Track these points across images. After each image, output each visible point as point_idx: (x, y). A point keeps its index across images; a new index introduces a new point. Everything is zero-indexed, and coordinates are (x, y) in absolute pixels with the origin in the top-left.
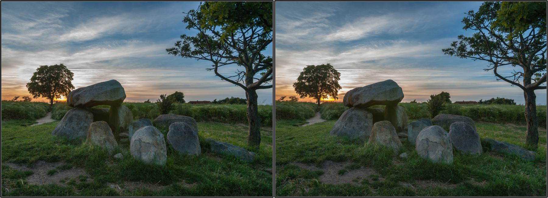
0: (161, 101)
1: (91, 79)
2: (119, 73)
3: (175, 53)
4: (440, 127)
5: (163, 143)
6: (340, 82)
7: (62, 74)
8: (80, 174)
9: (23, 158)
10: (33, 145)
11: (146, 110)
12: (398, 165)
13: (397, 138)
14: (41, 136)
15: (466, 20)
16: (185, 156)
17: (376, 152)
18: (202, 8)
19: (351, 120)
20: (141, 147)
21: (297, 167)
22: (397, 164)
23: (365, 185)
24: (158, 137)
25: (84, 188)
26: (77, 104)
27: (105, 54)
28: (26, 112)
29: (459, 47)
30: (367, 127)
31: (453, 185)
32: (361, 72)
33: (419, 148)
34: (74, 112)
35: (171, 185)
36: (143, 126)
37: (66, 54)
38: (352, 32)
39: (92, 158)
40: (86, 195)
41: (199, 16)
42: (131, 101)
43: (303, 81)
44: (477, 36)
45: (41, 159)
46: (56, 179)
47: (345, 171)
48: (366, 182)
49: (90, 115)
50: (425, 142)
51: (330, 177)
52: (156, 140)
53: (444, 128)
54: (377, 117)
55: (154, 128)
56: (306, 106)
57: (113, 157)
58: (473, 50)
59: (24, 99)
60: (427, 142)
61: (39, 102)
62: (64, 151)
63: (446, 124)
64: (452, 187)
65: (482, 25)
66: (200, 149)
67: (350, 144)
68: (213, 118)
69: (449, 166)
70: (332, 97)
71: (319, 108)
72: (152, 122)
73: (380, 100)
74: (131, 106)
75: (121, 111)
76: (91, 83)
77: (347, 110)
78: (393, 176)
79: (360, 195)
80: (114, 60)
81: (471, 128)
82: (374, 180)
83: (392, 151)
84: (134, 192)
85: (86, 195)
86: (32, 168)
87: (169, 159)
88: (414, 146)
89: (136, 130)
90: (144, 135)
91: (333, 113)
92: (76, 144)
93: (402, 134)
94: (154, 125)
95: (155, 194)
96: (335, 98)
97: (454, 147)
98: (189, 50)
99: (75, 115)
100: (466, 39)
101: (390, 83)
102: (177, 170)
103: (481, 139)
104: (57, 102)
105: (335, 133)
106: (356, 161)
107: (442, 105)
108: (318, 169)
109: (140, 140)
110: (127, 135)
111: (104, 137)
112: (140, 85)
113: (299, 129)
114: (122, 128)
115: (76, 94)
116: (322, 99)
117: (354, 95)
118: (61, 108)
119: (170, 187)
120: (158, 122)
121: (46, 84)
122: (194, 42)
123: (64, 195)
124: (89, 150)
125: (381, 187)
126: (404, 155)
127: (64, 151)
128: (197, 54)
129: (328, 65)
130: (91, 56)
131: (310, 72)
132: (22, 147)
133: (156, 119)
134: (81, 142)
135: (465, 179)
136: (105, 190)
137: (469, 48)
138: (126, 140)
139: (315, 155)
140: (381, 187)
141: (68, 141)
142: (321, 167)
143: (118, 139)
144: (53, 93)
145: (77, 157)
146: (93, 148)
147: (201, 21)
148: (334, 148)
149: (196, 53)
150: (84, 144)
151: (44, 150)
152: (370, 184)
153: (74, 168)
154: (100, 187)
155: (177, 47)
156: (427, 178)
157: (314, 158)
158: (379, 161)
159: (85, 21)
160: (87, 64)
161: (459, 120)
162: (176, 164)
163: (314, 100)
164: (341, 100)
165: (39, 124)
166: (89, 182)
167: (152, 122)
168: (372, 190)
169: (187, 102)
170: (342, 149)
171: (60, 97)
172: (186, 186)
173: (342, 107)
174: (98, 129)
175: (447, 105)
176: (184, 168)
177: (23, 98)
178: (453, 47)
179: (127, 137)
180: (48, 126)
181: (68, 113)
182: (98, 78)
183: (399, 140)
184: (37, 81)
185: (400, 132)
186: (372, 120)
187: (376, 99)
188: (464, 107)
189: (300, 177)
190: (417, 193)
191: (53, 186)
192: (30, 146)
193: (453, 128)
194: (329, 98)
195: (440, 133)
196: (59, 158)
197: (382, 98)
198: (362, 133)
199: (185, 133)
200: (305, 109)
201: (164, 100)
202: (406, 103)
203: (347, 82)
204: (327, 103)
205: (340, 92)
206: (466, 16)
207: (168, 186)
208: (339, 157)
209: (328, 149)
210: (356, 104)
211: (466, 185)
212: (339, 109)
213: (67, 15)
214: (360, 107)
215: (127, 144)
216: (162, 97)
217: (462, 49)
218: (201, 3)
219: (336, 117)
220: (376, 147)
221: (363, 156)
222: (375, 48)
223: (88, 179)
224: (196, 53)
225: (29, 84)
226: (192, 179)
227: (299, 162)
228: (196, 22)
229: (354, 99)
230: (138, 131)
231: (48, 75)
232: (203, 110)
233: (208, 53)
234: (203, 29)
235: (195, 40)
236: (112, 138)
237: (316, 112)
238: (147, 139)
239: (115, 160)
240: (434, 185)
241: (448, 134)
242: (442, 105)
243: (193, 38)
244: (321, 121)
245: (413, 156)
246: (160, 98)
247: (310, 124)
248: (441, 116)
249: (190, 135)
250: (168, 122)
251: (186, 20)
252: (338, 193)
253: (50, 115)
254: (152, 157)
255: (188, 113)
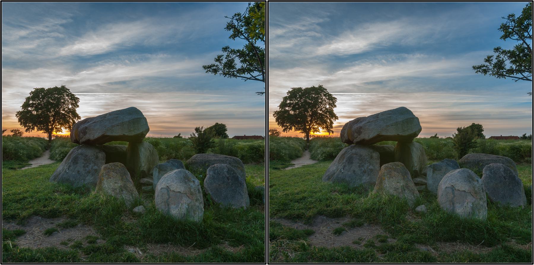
0: (197, 135)
1: (102, 106)
2: (140, 98)
3: (485, 72)
4: (470, 171)
5: (199, 192)
6: (336, 110)
7: (64, 99)
8: (88, 233)
9: (12, 213)
10: (25, 195)
11: (177, 149)
12: (413, 222)
13: (412, 185)
14: (36, 183)
15: (504, 27)
16: (228, 210)
17: (384, 204)
18: (251, 10)
19: (350, 161)
20: (454, 196)
21: (279, 225)
22: (412, 220)
23: (369, 249)
24: (192, 184)
25: (93, 252)
26: (84, 140)
27: (121, 72)
28: (277, 150)
29: (496, 64)
30: (372, 170)
31: (486, 249)
32: (364, 97)
33: (442, 199)
34: (80, 151)
35: (210, 249)
36: (172, 170)
37: (69, 72)
38: (95, 44)
39: (104, 213)
40: (96, 262)
41: (248, 22)
42: (156, 136)
43: (287, 108)
44: (520, 49)
45: (36, 213)
46: (55, 241)
47: (343, 230)
48: (371, 245)
49: (101, 155)
50: (450, 191)
51: (323, 237)
52: (190, 188)
53: (476, 173)
54: (386, 157)
55: (187, 171)
56: (291, 142)
57: (132, 211)
58: (514, 67)
59: (12, 133)
60: (453, 190)
61: (33, 137)
62: (66, 203)
63: (477, 167)
64: (485, 251)
65: (526, 34)
66: (248, 200)
67: (350, 194)
68: (526, 159)
69: (482, 223)
70: (325, 130)
71: (308, 145)
72: (184, 164)
73: (389, 134)
74: (155, 143)
75: (143, 150)
76: (102, 111)
77: (345, 148)
78: (407, 236)
79: (363, 261)
80: (390, 81)
81: (511, 172)
82: (382, 241)
83: (406, 203)
84: (160, 258)
85: (506, 261)
86: (23, 225)
87: (207, 213)
88: (436, 196)
89: (162, 175)
90: (173, 181)
91: (328, 152)
92: (82, 194)
93: (419, 180)
94: (187, 168)
95: (189, 261)
96: (329, 131)
97: (488, 197)
98: (233, 67)
99: (82, 154)
100: (504, 52)
101: (403, 111)
102: (217, 229)
103: (525, 187)
104: (57, 137)
105: (329, 179)
106: (358, 216)
107: (473, 141)
108: (306, 227)
109: (168, 188)
110: (151, 181)
111: (120, 184)
112: (168, 115)
113: (282, 174)
114: (143, 172)
115: (83, 126)
116: (312, 133)
117: (355, 127)
118: (63, 146)
119: (208, 251)
120: (192, 163)
121: (43, 112)
122: (240, 56)
123: (66, 262)
124: (100, 201)
125: (391, 251)
126: (421, 208)
127: (348, 203)
128: (244, 73)
129: (320, 87)
130: (359, 75)
131: (38, 97)
132: (10, 198)
133: (189, 161)
134: (88, 191)
135: (503, 240)
136: (122, 255)
137: (508, 64)
138: (150, 187)
139: (302, 209)
140: (391, 251)
141: (72, 190)
142: (311, 225)
143: (139, 186)
144: (52, 125)
145: (84, 210)
146: (105, 199)
147: (249, 28)
148: (327, 199)
149: (242, 71)
150: (93, 193)
151: (40, 201)
152: (377, 248)
153: (79, 225)
154: (114, 251)
155: (218, 63)
156: (452, 239)
157: (300, 214)
158: (388, 216)
159: (351, 28)
160: (98, 85)
161: (496, 161)
162: (216, 220)
163: (301, 135)
164: (337, 134)
165: (33, 166)
166: (99, 244)
167: (184, 164)
168: (379, 256)
169: (231, 137)
170: (339, 200)
171: (61, 131)
172: (230, 250)
173: (339, 143)
174: (112, 173)
175: (479, 140)
176: (510, 224)
177: (12, 131)
178: (487, 64)
179: (151, 184)
180: (45, 169)
181: (73, 152)
182: (369, 105)
183: (415, 189)
184: (30, 109)
185: (416, 177)
186: (379, 161)
187: (384, 133)
188: (502, 144)
189: (283, 238)
190: (439, 259)
191: (51, 250)
192: (21, 196)
193: (488, 172)
194: (322, 132)
195: (469, 179)
196: (60, 212)
197: (392, 132)
198: (366, 178)
199: (228, 178)
200: (289, 146)
201: (200, 135)
202: (425, 139)
203: (346, 109)
204: (318, 138)
205: (335, 123)
206: (505, 21)
207: (206, 250)
208: (335, 211)
209: (321, 201)
210: (358, 139)
211: (505, 248)
212: (334, 146)
213: (71, 21)
214: (363, 143)
215: (151, 194)
216: (197, 130)
217: (499, 65)
218: (250, 4)
219: (330, 157)
220: (385, 198)
221: (367, 210)
222: (383, 64)
223: (98, 241)
224: (242, 71)
225: (19, 113)
226: (238, 240)
227: (281, 217)
228: (243, 29)
229: (354, 131)
230: (166, 175)
231: (45, 101)
232: (252, 148)
233: (259, 71)
234: (252, 38)
235: (241, 54)
236: (131, 185)
237: (304, 151)
238: (177, 187)
239: (134, 215)
240: (461, 248)
241: (480, 180)
242: (473, 141)
243: (238, 51)
244: (311, 162)
245: (433, 210)
246: (195, 132)
247: (296, 166)
248: (470, 155)
249: (235, 181)
250: (205, 164)
251: (230, 26)
252: (333, 259)
253: (47, 155)
254: (184, 211)
255: (232, 152)
